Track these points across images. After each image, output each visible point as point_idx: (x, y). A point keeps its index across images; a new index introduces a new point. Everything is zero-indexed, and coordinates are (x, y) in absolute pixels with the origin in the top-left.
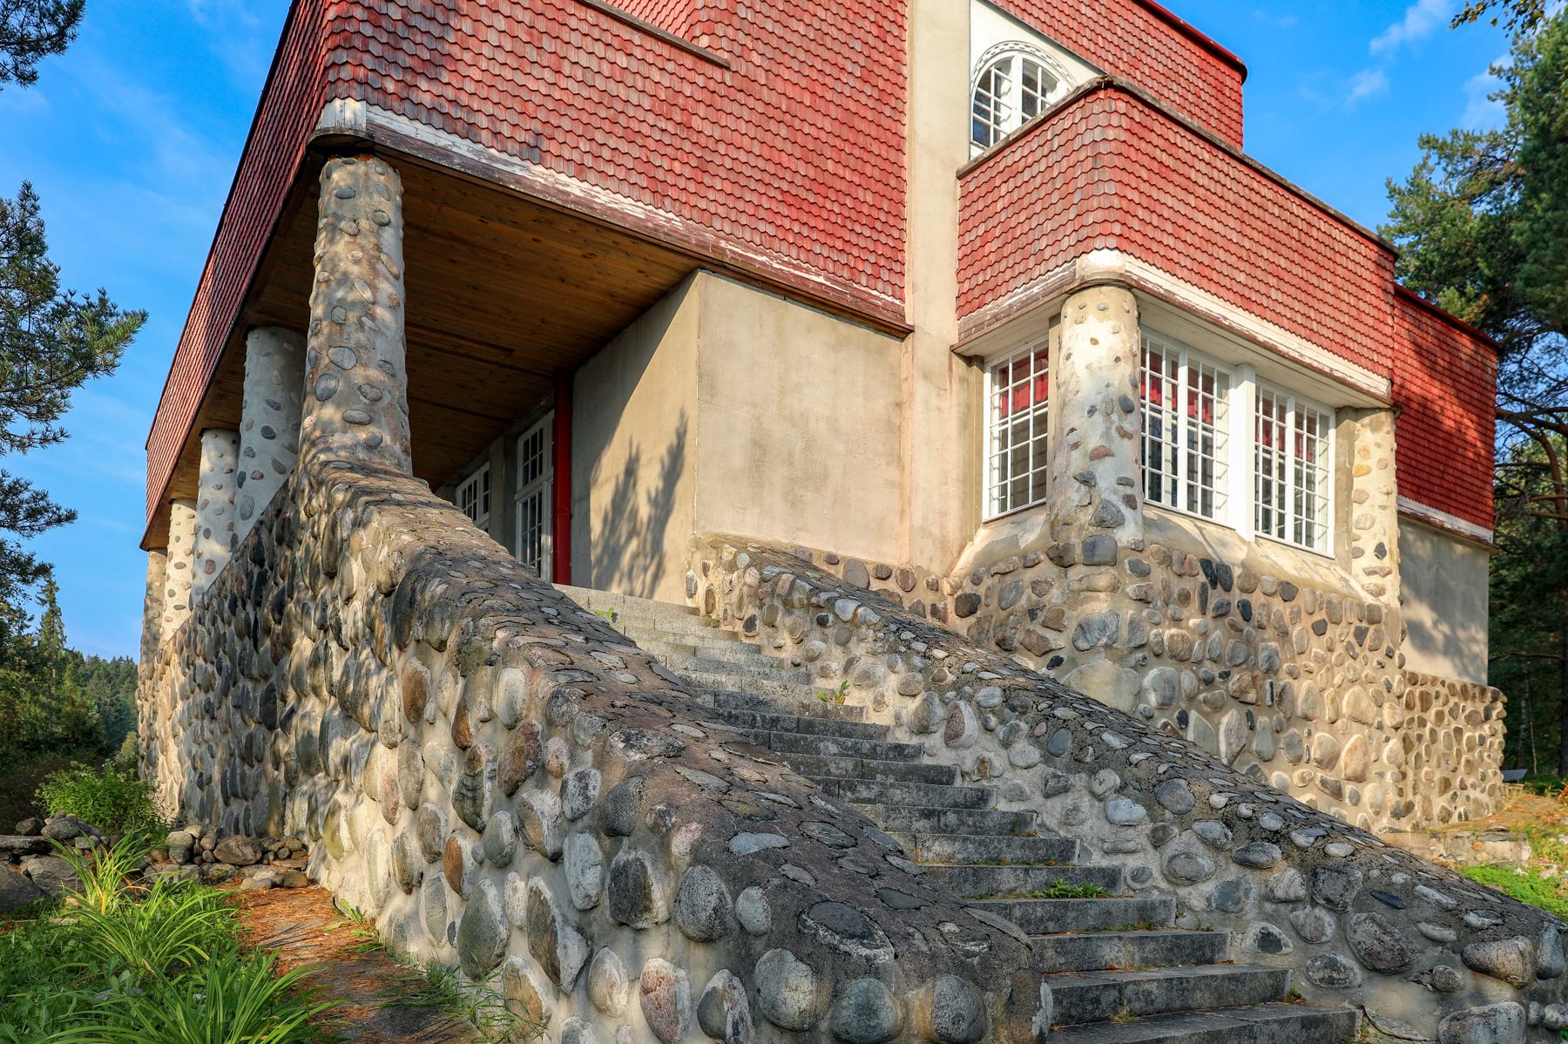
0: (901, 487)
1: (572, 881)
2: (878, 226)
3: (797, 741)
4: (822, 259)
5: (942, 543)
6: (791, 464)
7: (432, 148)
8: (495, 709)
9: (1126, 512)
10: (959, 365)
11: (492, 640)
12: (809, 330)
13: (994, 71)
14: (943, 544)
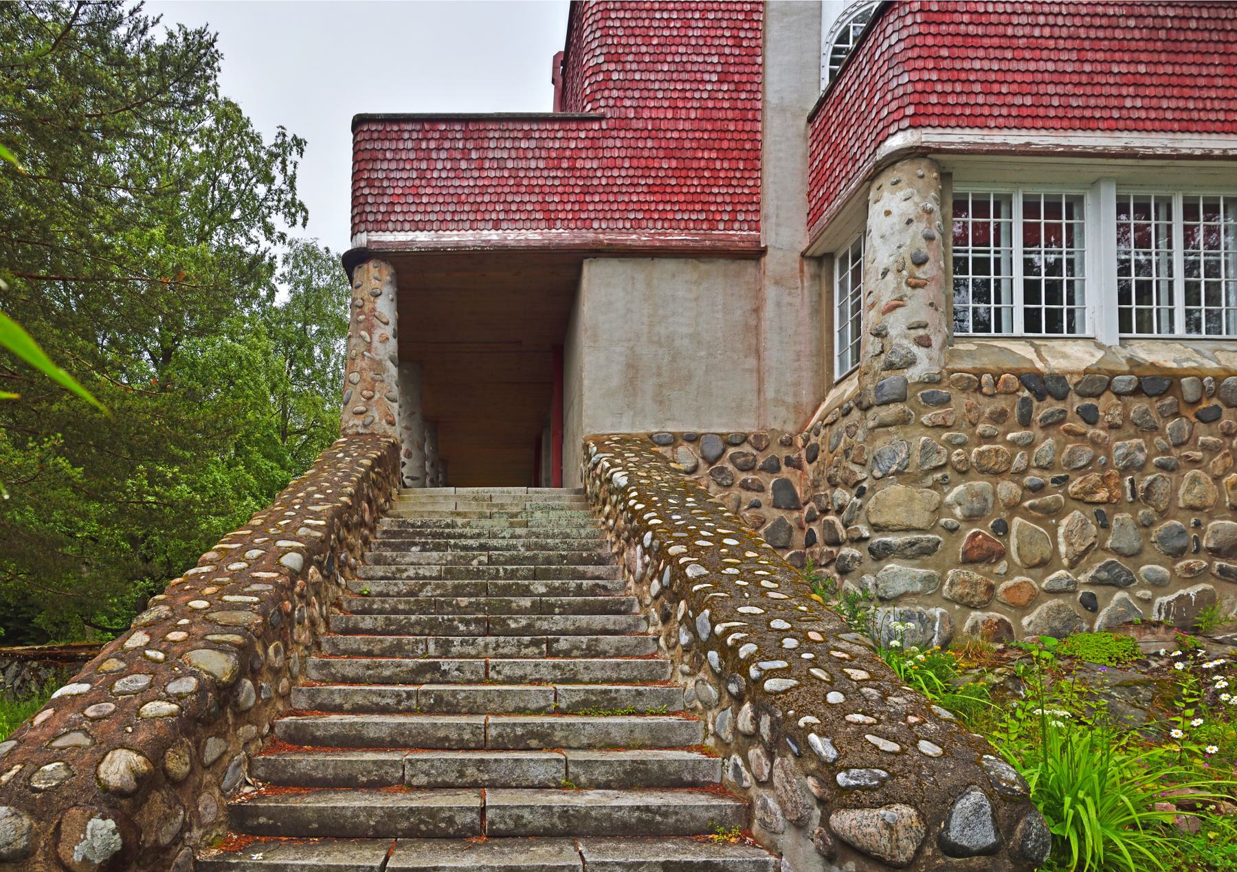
0: (759, 371)
1: (870, 319)
2: (734, 182)
3: (510, 586)
4: (1168, 21)
5: (795, 407)
6: (659, 375)
7: (405, 243)
8: (572, 848)
9: (920, 352)
10: (809, 269)
11: (179, 147)
12: (673, 276)
13: (852, 25)
14: (797, 408)
